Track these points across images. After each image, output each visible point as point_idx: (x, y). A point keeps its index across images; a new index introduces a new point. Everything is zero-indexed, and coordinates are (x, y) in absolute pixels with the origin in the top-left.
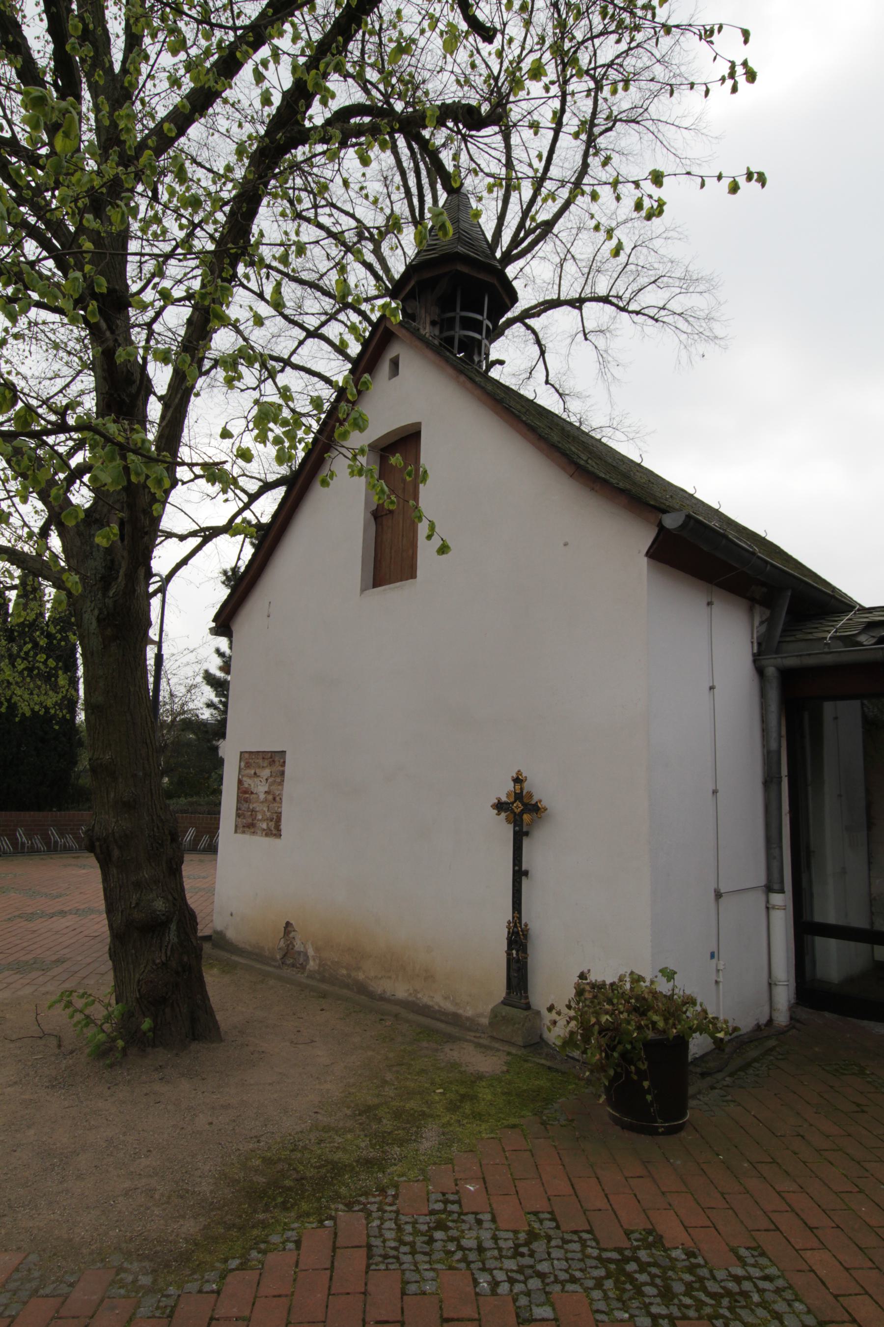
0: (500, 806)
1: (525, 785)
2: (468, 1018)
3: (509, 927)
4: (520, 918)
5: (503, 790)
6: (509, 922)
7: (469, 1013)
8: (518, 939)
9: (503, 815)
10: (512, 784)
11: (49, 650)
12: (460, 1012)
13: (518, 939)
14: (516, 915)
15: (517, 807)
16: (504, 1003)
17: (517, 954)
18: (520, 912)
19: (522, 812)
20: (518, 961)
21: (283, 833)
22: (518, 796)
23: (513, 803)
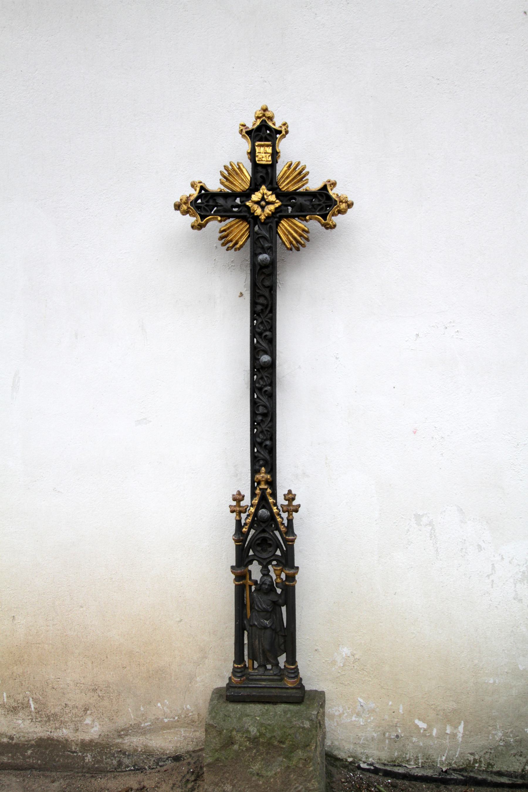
0: (205, 205)
1: (284, 146)
2: (86, 746)
3: (237, 509)
4: (272, 484)
5: (217, 156)
6: (238, 498)
7: (93, 729)
8: (264, 536)
9: (215, 226)
10: (246, 145)
11: (350, 781)
12: (65, 733)
13: (264, 536)
14: (263, 475)
15: (263, 203)
16: (232, 694)
17: (265, 573)
18: (272, 469)
19: (265, 217)
20: (266, 588)
21: (350, 199)
22: (264, 175)
23: (274, 188)
